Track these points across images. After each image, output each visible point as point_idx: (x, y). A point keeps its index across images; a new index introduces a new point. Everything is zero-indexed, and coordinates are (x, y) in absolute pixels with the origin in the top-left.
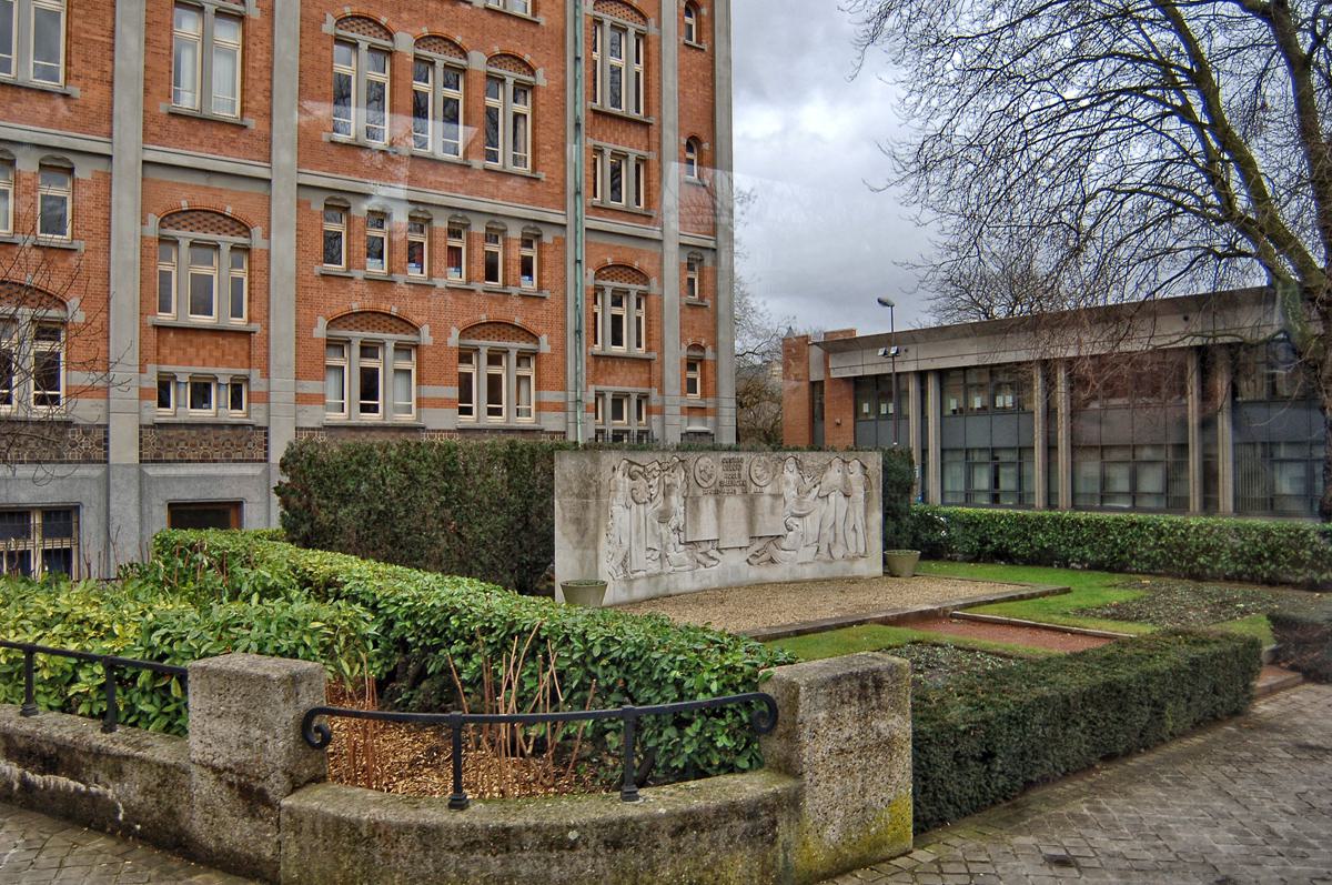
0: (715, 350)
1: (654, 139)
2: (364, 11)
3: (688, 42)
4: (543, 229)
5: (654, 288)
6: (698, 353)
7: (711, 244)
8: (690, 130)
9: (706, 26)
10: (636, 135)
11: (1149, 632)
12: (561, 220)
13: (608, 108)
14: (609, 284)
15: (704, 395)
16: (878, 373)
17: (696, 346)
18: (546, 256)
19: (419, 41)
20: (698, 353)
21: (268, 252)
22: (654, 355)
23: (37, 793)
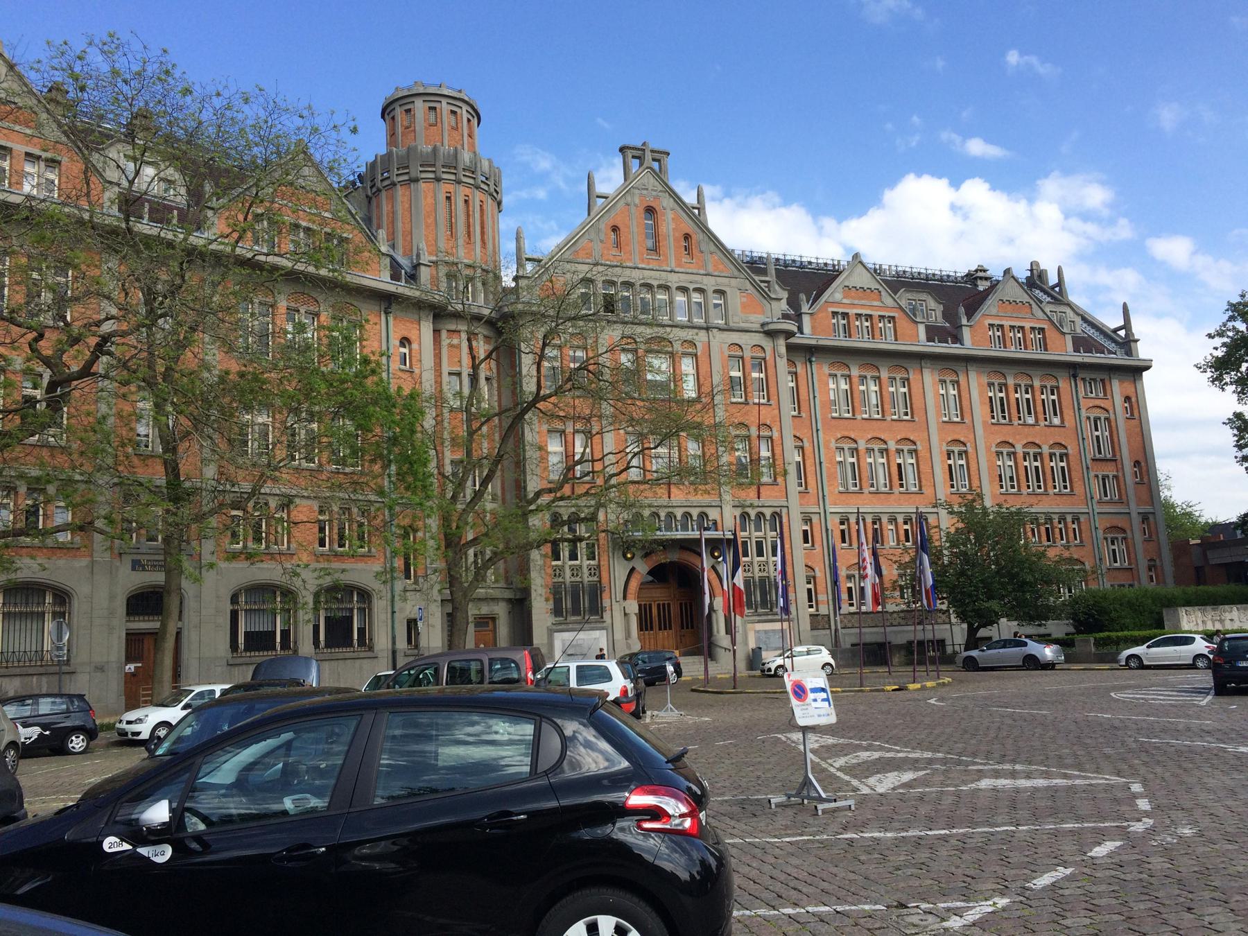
0: (1161, 560)
1: (1120, 466)
2: (1004, 439)
3: (403, 367)
4: (849, 515)
5: (1129, 535)
6: (1152, 563)
7: (1152, 511)
8: (1134, 459)
9: (1135, 406)
10: (1111, 466)
11: (1095, 850)
12: (1087, 511)
13: (1098, 456)
14: (1109, 536)
15: (1158, 583)
16: (534, 617)
17: (1151, 560)
18: (1083, 527)
19: (898, 442)
20: (1152, 563)
21: (200, 554)
22: (1133, 566)
23: (174, 805)
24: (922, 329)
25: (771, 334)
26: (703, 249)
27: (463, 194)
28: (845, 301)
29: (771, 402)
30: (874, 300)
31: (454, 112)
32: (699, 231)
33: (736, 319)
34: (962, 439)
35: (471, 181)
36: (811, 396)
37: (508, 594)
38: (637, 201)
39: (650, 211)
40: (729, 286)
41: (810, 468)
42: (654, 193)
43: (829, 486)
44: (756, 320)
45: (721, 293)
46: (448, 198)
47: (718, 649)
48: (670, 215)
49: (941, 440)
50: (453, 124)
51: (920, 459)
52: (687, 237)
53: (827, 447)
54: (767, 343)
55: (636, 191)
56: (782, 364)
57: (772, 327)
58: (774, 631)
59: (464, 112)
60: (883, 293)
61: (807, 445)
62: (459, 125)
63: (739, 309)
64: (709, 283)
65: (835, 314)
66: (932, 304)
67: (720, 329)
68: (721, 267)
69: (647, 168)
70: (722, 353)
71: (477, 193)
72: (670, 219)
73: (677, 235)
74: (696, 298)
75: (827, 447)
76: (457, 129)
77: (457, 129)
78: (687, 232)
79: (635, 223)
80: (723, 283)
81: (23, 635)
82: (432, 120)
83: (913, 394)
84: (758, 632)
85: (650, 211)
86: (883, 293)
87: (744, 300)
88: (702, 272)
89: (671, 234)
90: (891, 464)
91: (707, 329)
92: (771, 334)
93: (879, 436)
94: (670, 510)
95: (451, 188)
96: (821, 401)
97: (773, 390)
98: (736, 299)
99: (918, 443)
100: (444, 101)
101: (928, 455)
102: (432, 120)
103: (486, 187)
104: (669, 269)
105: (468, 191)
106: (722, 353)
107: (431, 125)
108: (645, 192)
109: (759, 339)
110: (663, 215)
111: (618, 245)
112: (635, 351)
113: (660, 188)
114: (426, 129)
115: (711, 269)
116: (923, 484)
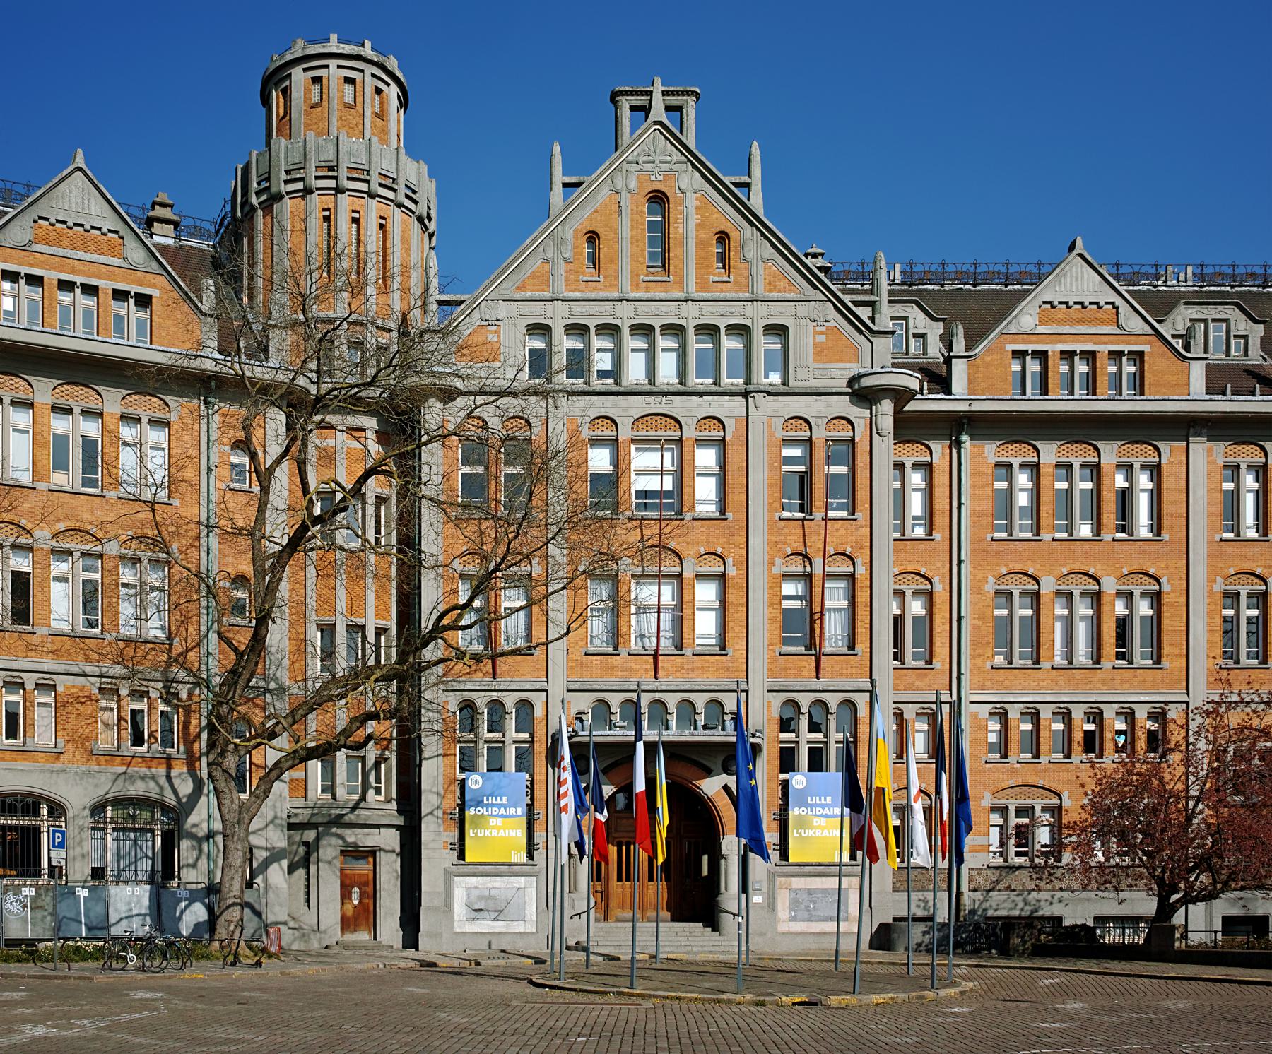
24: (1198, 372)
25: (863, 395)
26: (749, 256)
27: (349, 209)
28: (1041, 330)
29: (858, 515)
30: (1103, 323)
31: (378, 91)
32: (745, 224)
33: (802, 374)
34: (1259, 571)
35: (364, 187)
36: (955, 504)
37: (400, 821)
38: (633, 185)
39: (658, 199)
40: (795, 316)
41: (940, 627)
42: (665, 167)
43: (973, 658)
44: (839, 374)
45: (778, 330)
46: (327, 219)
47: (723, 915)
48: (693, 202)
49: (1212, 575)
50: (349, 99)
51: (1164, 608)
52: (723, 238)
53: (977, 588)
54: (860, 415)
55: (634, 167)
56: (886, 450)
57: (866, 382)
58: (824, 891)
59: (368, 78)
60: (1124, 308)
61: (939, 588)
62: (359, 100)
63: (810, 358)
64: (757, 317)
65: (1020, 355)
66: (1241, 324)
67: (769, 394)
68: (782, 284)
69: (655, 123)
70: (772, 434)
71: (373, 203)
72: (692, 210)
73: (703, 235)
74: (730, 344)
75: (977, 588)
76: (354, 107)
77: (354, 107)
78: (723, 228)
79: (627, 222)
80: (781, 313)
81: (684, 1031)
82: (316, 98)
83: (1164, 491)
84: (796, 891)
85: (658, 199)
86: (1124, 308)
87: (822, 338)
88: (747, 295)
89: (692, 233)
90: (1104, 618)
91: (746, 395)
92: (863, 395)
93: (1084, 568)
94: (658, 696)
95: (329, 201)
96: (973, 512)
97: (862, 493)
98: (803, 339)
99: (1164, 580)
100: (333, 63)
101: (1183, 600)
102: (316, 98)
103: (390, 195)
104: (682, 295)
105: (358, 203)
106: (772, 434)
107: (312, 107)
108: (648, 167)
109: (842, 406)
110: (683, 202)
111: (595, 261)
112: (614, 442)
113: (676, 156)
114: (307, 114)
115: (761, 291)
116: (1164, 652)
